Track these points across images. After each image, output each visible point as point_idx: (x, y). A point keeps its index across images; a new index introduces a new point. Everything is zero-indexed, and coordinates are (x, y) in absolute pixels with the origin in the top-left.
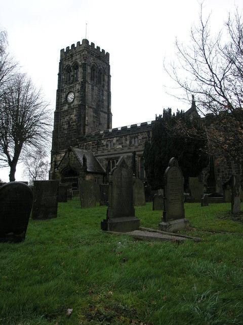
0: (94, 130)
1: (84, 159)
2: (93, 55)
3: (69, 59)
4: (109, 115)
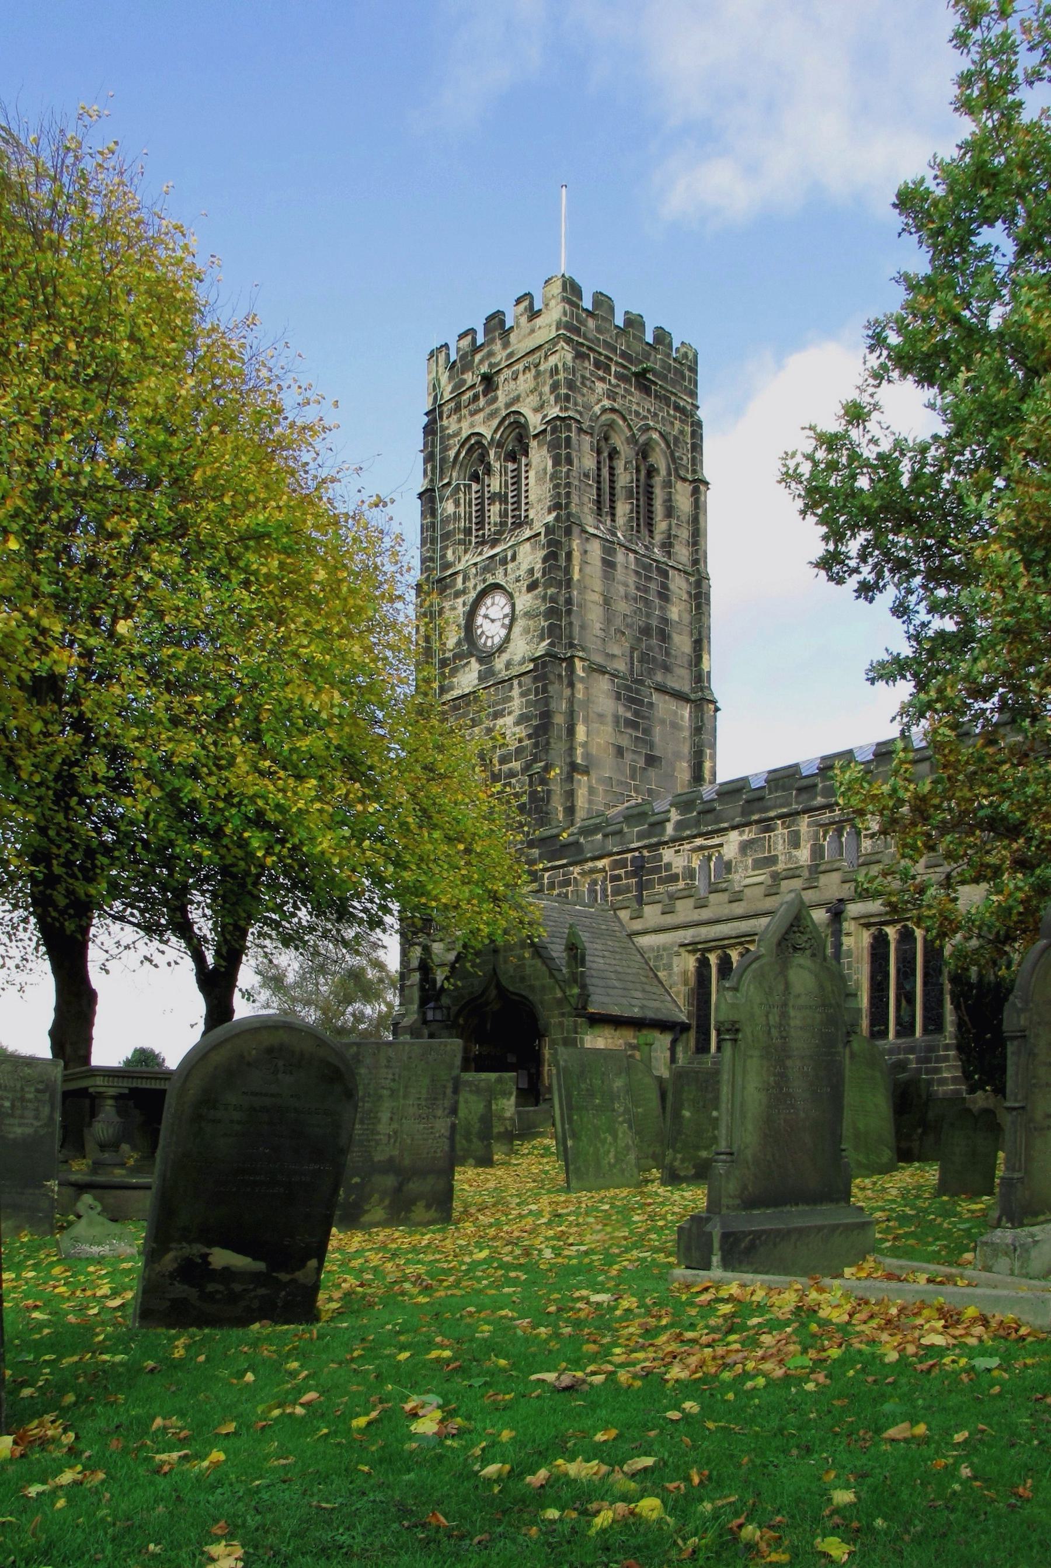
0: (622, 797)
2: (607, 369)
3: (476, 398)
4: (700, 701)
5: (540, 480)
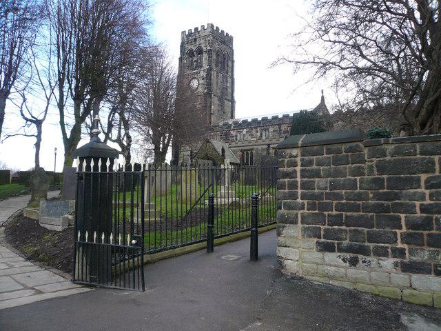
1: (223, 150)
5: (206, 59)
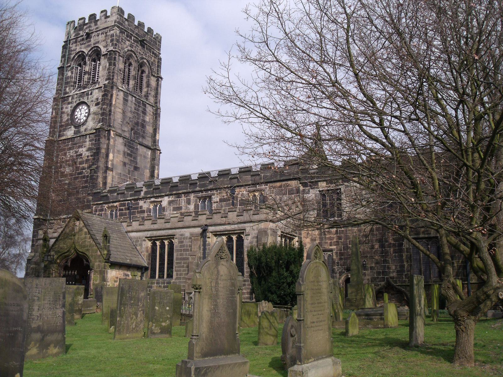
5: (104, 69)
